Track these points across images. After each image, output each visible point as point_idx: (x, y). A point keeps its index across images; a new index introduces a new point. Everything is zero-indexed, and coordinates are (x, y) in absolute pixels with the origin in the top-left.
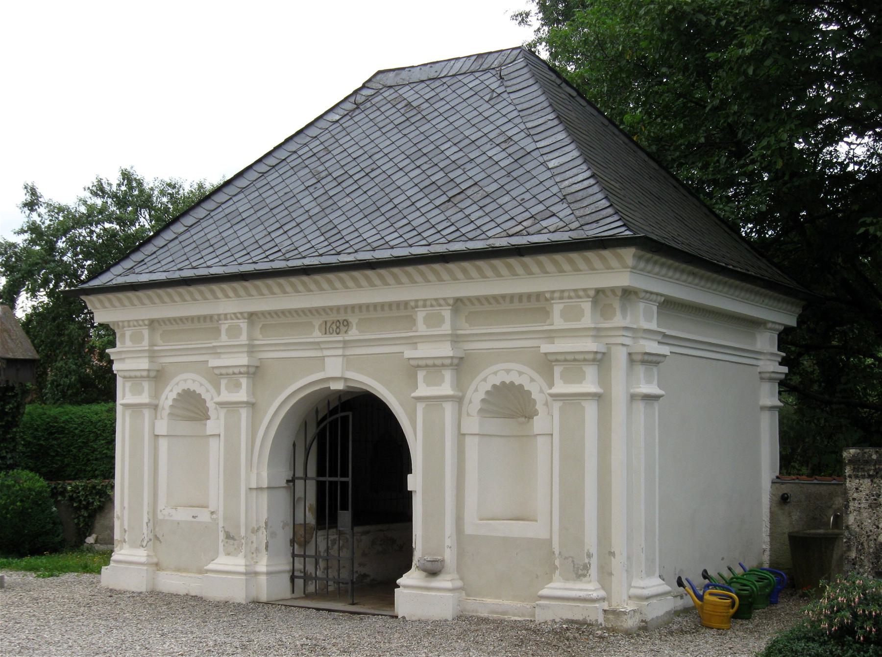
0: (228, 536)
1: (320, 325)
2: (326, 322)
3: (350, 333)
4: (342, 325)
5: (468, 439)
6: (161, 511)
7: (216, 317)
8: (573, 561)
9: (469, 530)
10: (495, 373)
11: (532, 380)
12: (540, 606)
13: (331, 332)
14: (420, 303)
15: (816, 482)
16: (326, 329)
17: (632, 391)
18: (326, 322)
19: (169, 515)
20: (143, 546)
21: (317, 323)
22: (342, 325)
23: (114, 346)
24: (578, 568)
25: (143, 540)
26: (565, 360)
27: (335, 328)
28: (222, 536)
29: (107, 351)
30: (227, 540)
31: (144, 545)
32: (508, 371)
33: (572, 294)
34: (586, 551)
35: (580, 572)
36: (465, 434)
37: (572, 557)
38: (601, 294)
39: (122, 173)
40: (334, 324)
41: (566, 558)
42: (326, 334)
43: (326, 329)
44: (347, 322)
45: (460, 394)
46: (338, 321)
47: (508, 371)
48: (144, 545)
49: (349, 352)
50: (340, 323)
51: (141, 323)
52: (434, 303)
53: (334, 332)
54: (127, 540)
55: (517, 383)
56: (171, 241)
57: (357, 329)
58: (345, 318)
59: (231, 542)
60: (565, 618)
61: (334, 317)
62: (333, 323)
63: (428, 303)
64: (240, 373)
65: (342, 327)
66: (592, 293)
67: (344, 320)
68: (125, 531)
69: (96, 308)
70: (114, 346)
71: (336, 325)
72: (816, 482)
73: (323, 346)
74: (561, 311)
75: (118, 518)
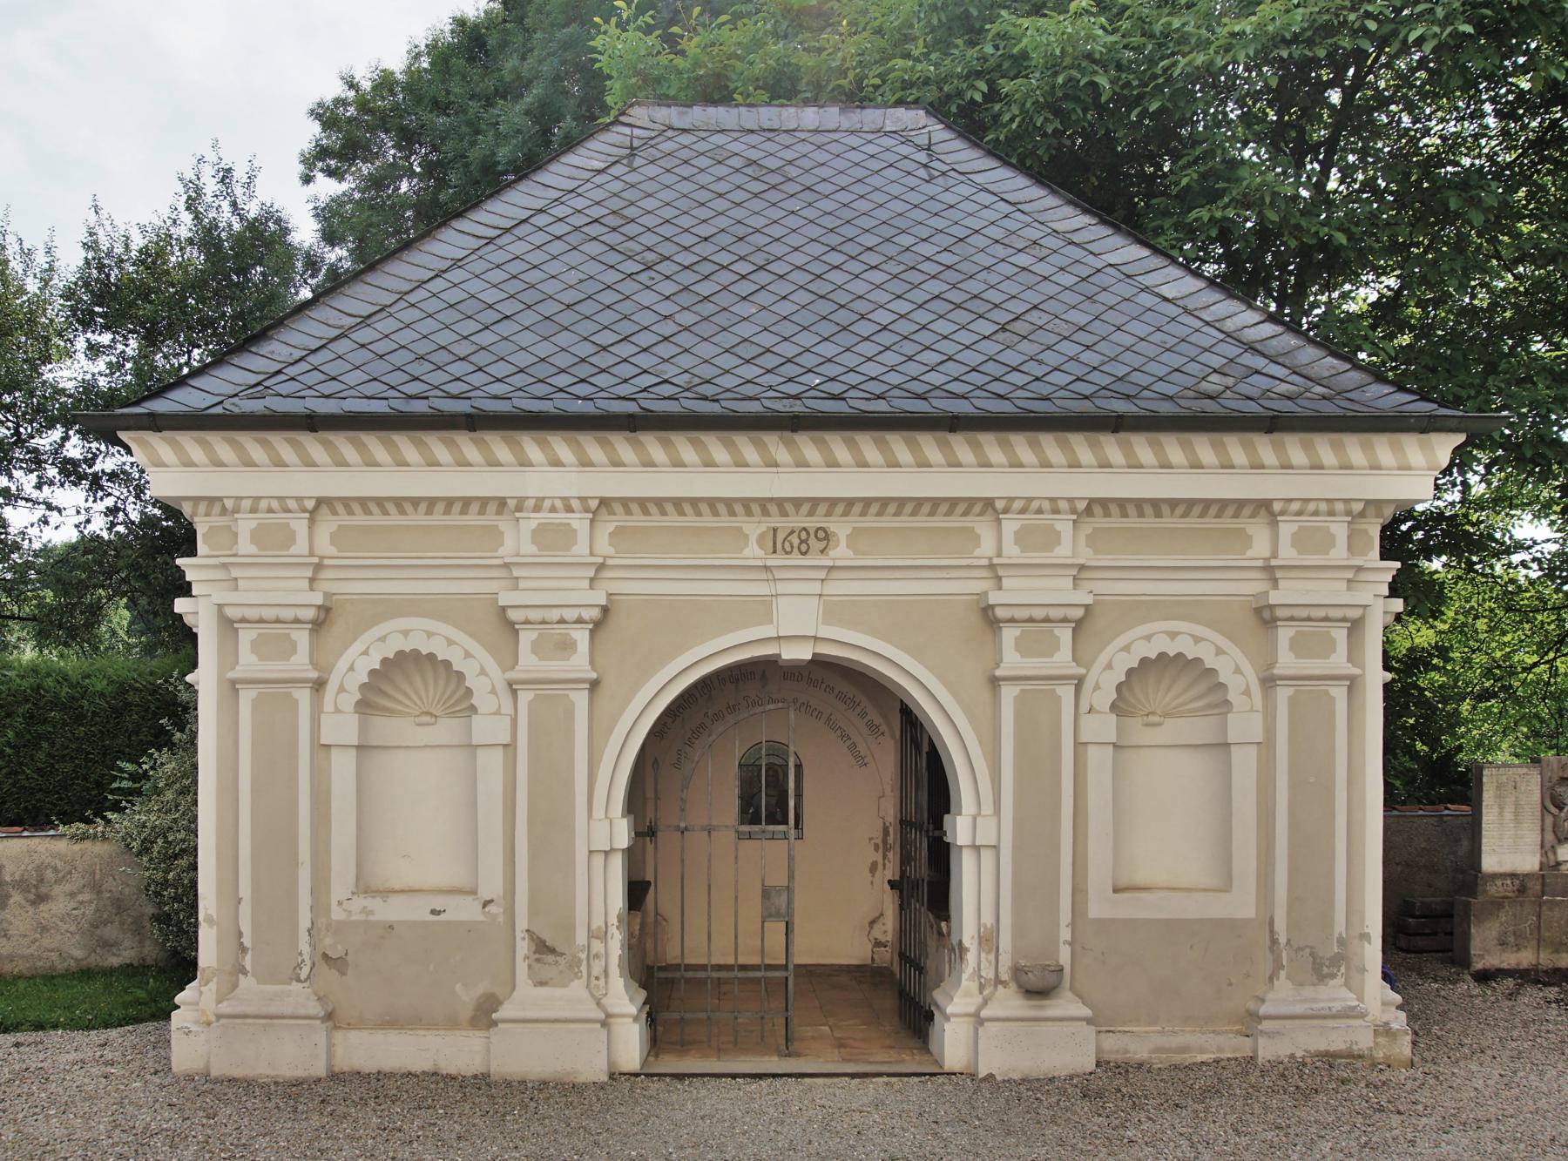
0: (542, 948)
1: (761, 538)
2: (775, 530)
3: (832, 553)
4: (812, 536)
5: (1091, 750)
6: (340, 903)
7: (512, 504)
8: (1312, 954)
9: (1095, 911)
10: (1148, 638)
11: (1220, 651)
12: (1266, 1033)
13: (788, 549)
14: (246, 504)
15: (1421, 812)
16: (775, 543)
17: (231, 675)
18: (775, 530)
19: (364, 910)
20: (299, 980)
21: (755, 528)
22: (812, 536)
23: (192, 552)
24: (1322, 965)
25: (299, 966)
26: (261, 621)
27: (796, 542)
28: (523, 947)
29: (179, 561)
30: (537, 956)
31: (303, 977)
32: (1173, 635)
33: (275, 504)
34: (1336, 935)
35: (1325, 970)
36: (329, 746)
37: (1311, 947)
38: (324, 509)
39: (317, 215)
40: (795, 535)
41: (1300, 949)
42: (775, 552)
43: (775, 543)
44: (826, 532)
45: (1082, 671)
46: (805, 529)
47: (1173, 635)
48: (303, 977)
49: (833, 588)
50: (808, 533)
51: (292, 504)
52: (275, 504)
53: (796, 550)
54: (248, 968)
55: (1172, 653)
56: (314, 351)
57: (1087, 546)
58: (822, 525)
59: (550, 958)
60: (1313, 1048)
61: (797, 521)
62: (792, 532)
63: (263, 504)
64: (297, 621)
65: (812, 541)
66: (594, 504)
67: (819, 529)
68: (243, 949)
69: (160, 464)
70: (192, 552)
71: (799, 537)
72: (1421, 812)
73: (778, 575)
74: (1016, 533)
75: (210, 921)
